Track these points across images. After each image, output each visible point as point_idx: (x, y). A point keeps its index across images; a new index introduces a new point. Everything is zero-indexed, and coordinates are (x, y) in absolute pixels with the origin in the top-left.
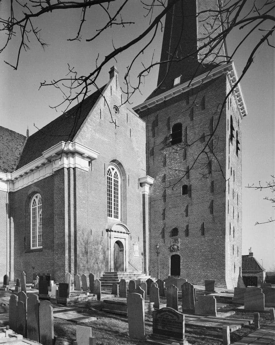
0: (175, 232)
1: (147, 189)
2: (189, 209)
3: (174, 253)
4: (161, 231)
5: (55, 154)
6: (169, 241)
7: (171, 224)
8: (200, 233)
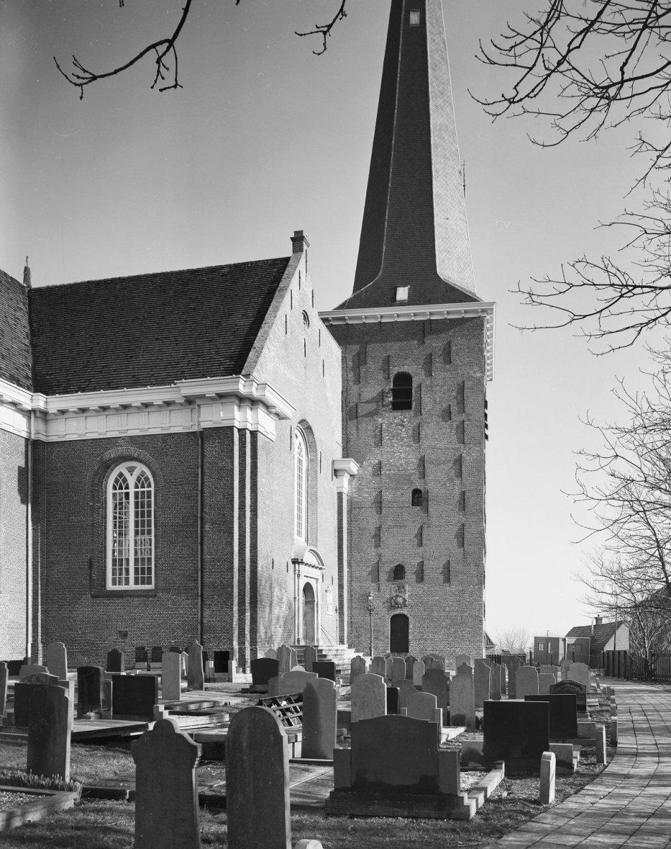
0: (399, 572)
1: (345, 484)
2: (425, 533)
3: (398, 612)
4: (370, 569)
5: (214, 395)
6: (388, 589)
7: (392, 556)
8: (441, 578)
